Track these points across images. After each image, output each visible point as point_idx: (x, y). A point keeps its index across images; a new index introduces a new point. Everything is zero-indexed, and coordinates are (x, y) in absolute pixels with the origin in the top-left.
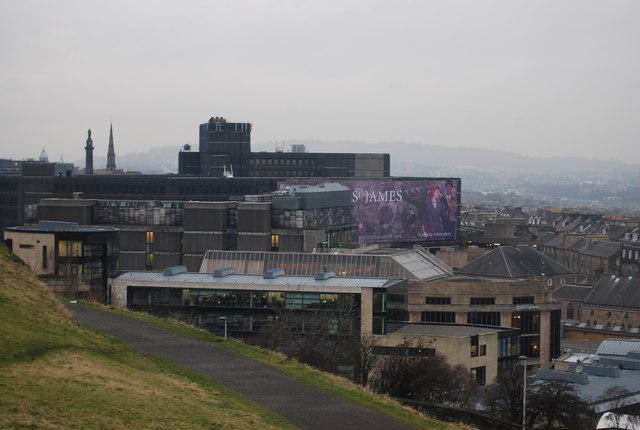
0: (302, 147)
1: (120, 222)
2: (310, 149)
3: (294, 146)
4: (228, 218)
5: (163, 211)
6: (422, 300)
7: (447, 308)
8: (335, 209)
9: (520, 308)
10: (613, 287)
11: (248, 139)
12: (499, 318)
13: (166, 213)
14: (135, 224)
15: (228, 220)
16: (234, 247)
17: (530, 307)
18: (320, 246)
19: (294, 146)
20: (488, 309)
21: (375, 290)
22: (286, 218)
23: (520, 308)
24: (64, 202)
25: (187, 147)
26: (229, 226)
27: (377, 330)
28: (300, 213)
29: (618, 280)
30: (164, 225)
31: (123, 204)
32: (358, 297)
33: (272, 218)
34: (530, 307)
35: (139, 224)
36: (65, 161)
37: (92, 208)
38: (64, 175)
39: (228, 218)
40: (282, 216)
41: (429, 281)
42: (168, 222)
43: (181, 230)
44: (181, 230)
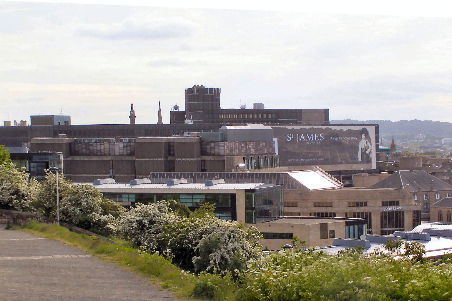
0: (261, 105)
2: (268, 106)
3: (255, 105)
4: (169, 149)
5: (121, 145)
6: (311, 204)
7: (329, 210)
9: (387, 209)
11: (218, 100)
12: (403, 215)
13: (124, 147)
16: (173, 169)
19: (255, 105)
20: (362, 209)
22: (211, 148)
23: (387, 209)
24: (56, 140)
25: (176, 107)
26: (170, 154)
30: (123, 155)
31: (94, 140)
32: (233, 197)
33: (201, 148)
35: (105, 155)
36: (65, 114)
37: (70, 144)
38: (63, 124)
39: (169, 149)
41: (322, 192)
42: (125, 153)
43: (134, 158)
44: (134, 158)
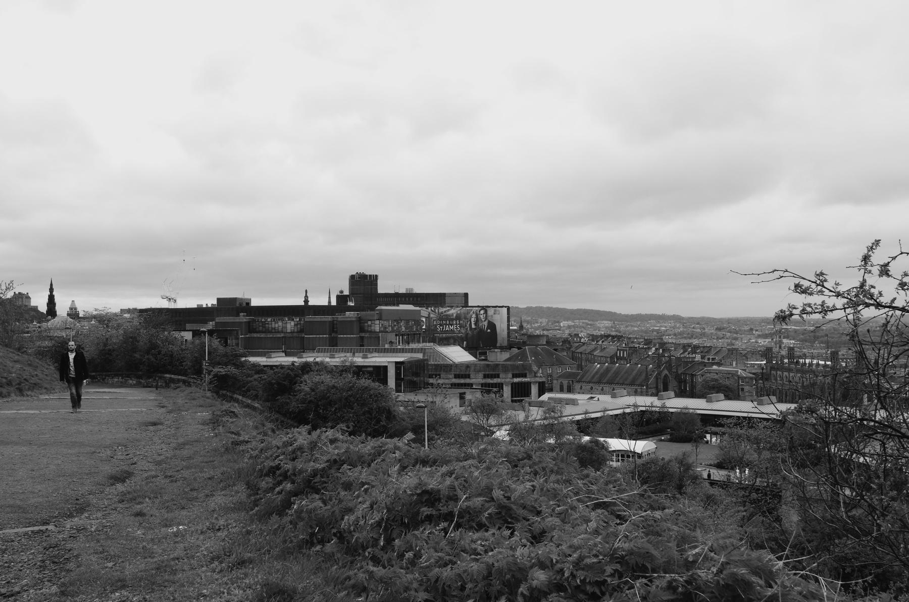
0: (412, 289)
1: (267, 331)
3: (407, 289)
5: (293, 323)
7: (467, 381)
8: (407, 321)
9: (516, 380)
10: (595, 370)
14: (275, 332)
15: (333, 328)
17: (524, 380)
18: (391, 343)
19: (407, 289)
21: (397, 363)
22: (368, 326)
23: (516, 380)
25: (342, 292)
26: (333, 331)
27: (398, 390)
28: (377, 322)
29: (599, 366)
30: (294, 332)
32: (386, 368)
34: (524, 380)
35: (278, 332)
37: (249, 322)
40: (366, 324)
42: (296, 330)
